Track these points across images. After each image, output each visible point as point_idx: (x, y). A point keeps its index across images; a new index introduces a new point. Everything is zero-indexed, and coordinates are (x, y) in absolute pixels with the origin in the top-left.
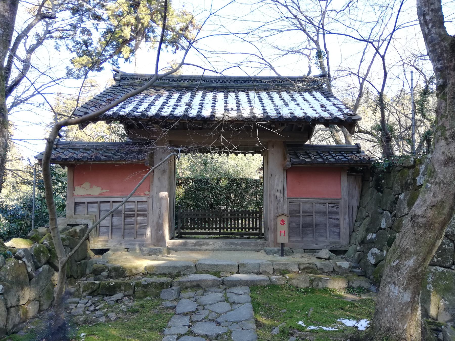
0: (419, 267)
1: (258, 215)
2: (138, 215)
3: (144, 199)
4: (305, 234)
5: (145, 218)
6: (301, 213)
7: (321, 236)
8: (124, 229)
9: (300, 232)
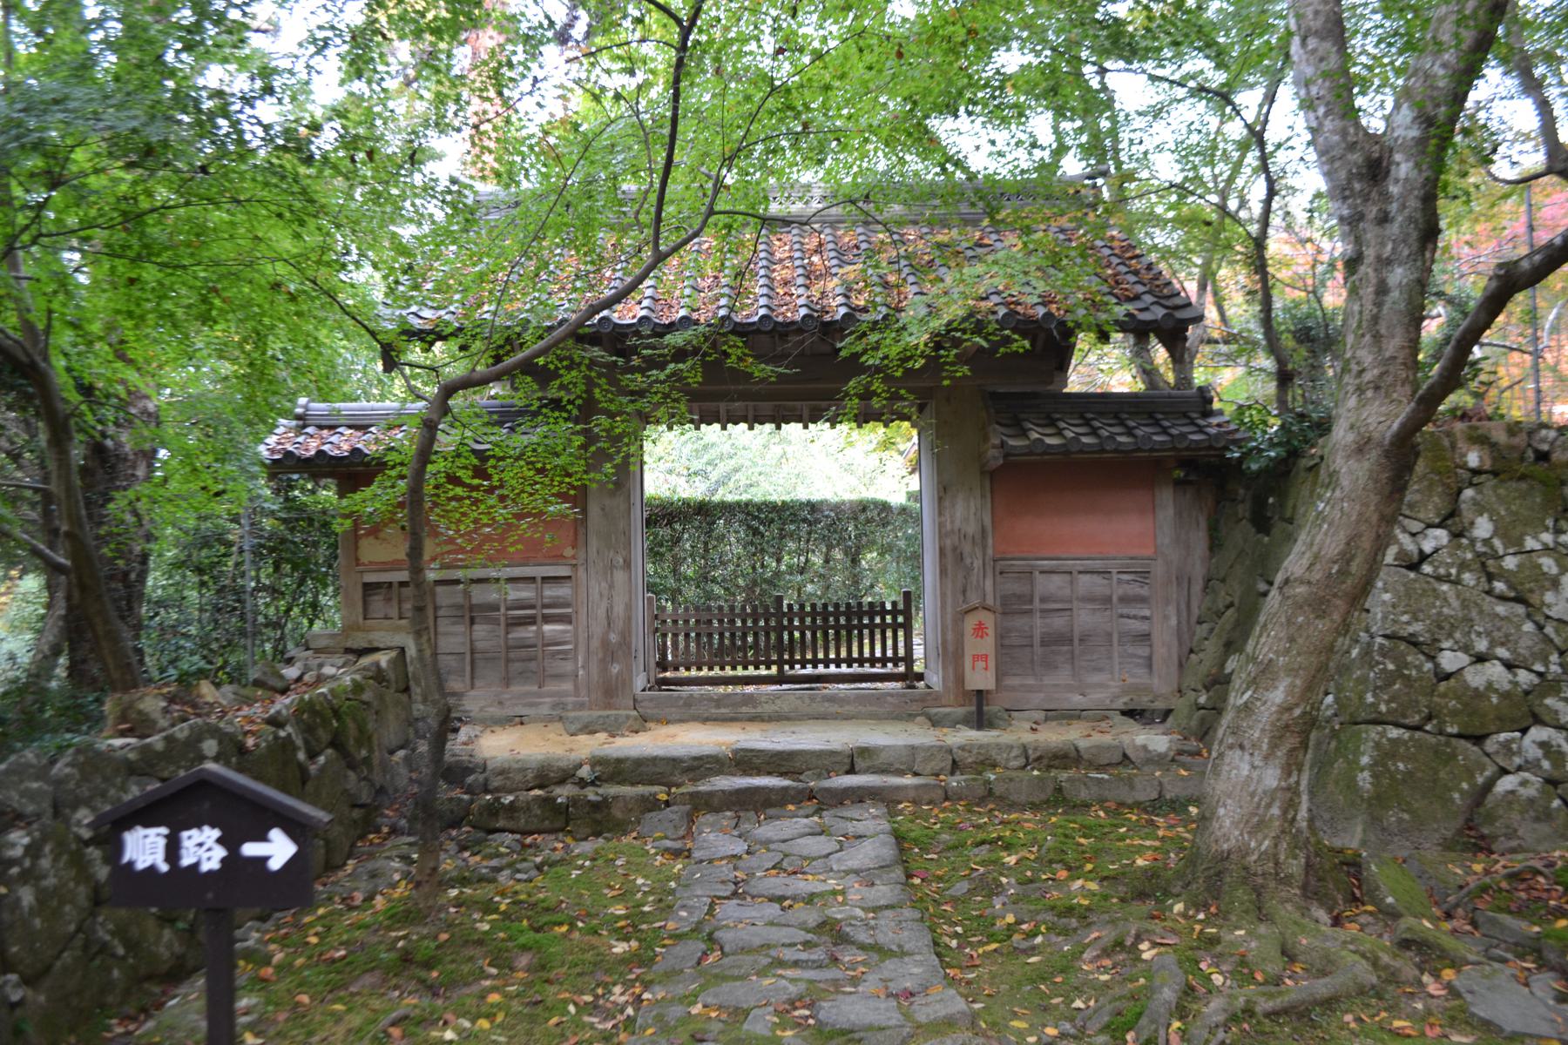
0: (1297, 705)
1: (900, 619)
2: (548, 619)
3: (563, 571)
4: (1050, 666)
5: (569, 627)
6: (1037, 604)
7: (1100, 670)
8: (508, 661)
9: (1032, 661)
